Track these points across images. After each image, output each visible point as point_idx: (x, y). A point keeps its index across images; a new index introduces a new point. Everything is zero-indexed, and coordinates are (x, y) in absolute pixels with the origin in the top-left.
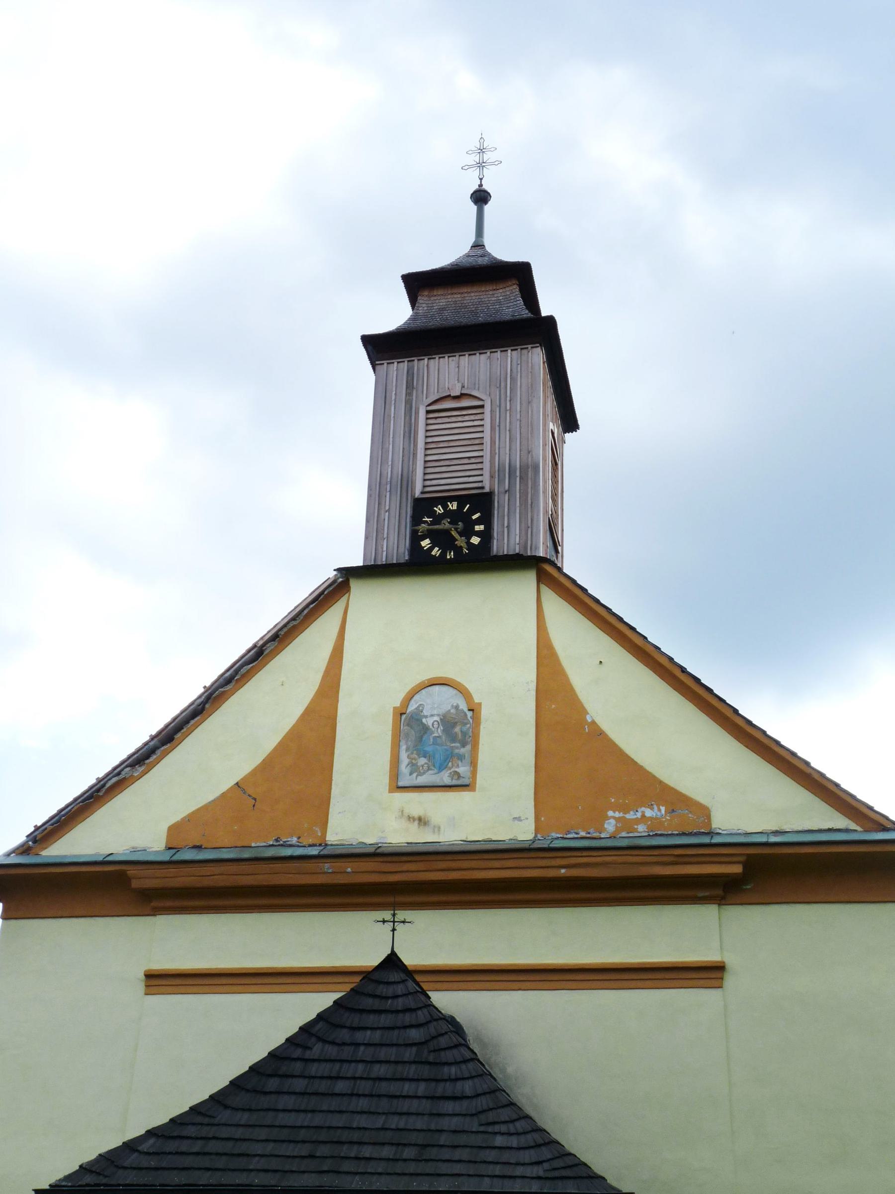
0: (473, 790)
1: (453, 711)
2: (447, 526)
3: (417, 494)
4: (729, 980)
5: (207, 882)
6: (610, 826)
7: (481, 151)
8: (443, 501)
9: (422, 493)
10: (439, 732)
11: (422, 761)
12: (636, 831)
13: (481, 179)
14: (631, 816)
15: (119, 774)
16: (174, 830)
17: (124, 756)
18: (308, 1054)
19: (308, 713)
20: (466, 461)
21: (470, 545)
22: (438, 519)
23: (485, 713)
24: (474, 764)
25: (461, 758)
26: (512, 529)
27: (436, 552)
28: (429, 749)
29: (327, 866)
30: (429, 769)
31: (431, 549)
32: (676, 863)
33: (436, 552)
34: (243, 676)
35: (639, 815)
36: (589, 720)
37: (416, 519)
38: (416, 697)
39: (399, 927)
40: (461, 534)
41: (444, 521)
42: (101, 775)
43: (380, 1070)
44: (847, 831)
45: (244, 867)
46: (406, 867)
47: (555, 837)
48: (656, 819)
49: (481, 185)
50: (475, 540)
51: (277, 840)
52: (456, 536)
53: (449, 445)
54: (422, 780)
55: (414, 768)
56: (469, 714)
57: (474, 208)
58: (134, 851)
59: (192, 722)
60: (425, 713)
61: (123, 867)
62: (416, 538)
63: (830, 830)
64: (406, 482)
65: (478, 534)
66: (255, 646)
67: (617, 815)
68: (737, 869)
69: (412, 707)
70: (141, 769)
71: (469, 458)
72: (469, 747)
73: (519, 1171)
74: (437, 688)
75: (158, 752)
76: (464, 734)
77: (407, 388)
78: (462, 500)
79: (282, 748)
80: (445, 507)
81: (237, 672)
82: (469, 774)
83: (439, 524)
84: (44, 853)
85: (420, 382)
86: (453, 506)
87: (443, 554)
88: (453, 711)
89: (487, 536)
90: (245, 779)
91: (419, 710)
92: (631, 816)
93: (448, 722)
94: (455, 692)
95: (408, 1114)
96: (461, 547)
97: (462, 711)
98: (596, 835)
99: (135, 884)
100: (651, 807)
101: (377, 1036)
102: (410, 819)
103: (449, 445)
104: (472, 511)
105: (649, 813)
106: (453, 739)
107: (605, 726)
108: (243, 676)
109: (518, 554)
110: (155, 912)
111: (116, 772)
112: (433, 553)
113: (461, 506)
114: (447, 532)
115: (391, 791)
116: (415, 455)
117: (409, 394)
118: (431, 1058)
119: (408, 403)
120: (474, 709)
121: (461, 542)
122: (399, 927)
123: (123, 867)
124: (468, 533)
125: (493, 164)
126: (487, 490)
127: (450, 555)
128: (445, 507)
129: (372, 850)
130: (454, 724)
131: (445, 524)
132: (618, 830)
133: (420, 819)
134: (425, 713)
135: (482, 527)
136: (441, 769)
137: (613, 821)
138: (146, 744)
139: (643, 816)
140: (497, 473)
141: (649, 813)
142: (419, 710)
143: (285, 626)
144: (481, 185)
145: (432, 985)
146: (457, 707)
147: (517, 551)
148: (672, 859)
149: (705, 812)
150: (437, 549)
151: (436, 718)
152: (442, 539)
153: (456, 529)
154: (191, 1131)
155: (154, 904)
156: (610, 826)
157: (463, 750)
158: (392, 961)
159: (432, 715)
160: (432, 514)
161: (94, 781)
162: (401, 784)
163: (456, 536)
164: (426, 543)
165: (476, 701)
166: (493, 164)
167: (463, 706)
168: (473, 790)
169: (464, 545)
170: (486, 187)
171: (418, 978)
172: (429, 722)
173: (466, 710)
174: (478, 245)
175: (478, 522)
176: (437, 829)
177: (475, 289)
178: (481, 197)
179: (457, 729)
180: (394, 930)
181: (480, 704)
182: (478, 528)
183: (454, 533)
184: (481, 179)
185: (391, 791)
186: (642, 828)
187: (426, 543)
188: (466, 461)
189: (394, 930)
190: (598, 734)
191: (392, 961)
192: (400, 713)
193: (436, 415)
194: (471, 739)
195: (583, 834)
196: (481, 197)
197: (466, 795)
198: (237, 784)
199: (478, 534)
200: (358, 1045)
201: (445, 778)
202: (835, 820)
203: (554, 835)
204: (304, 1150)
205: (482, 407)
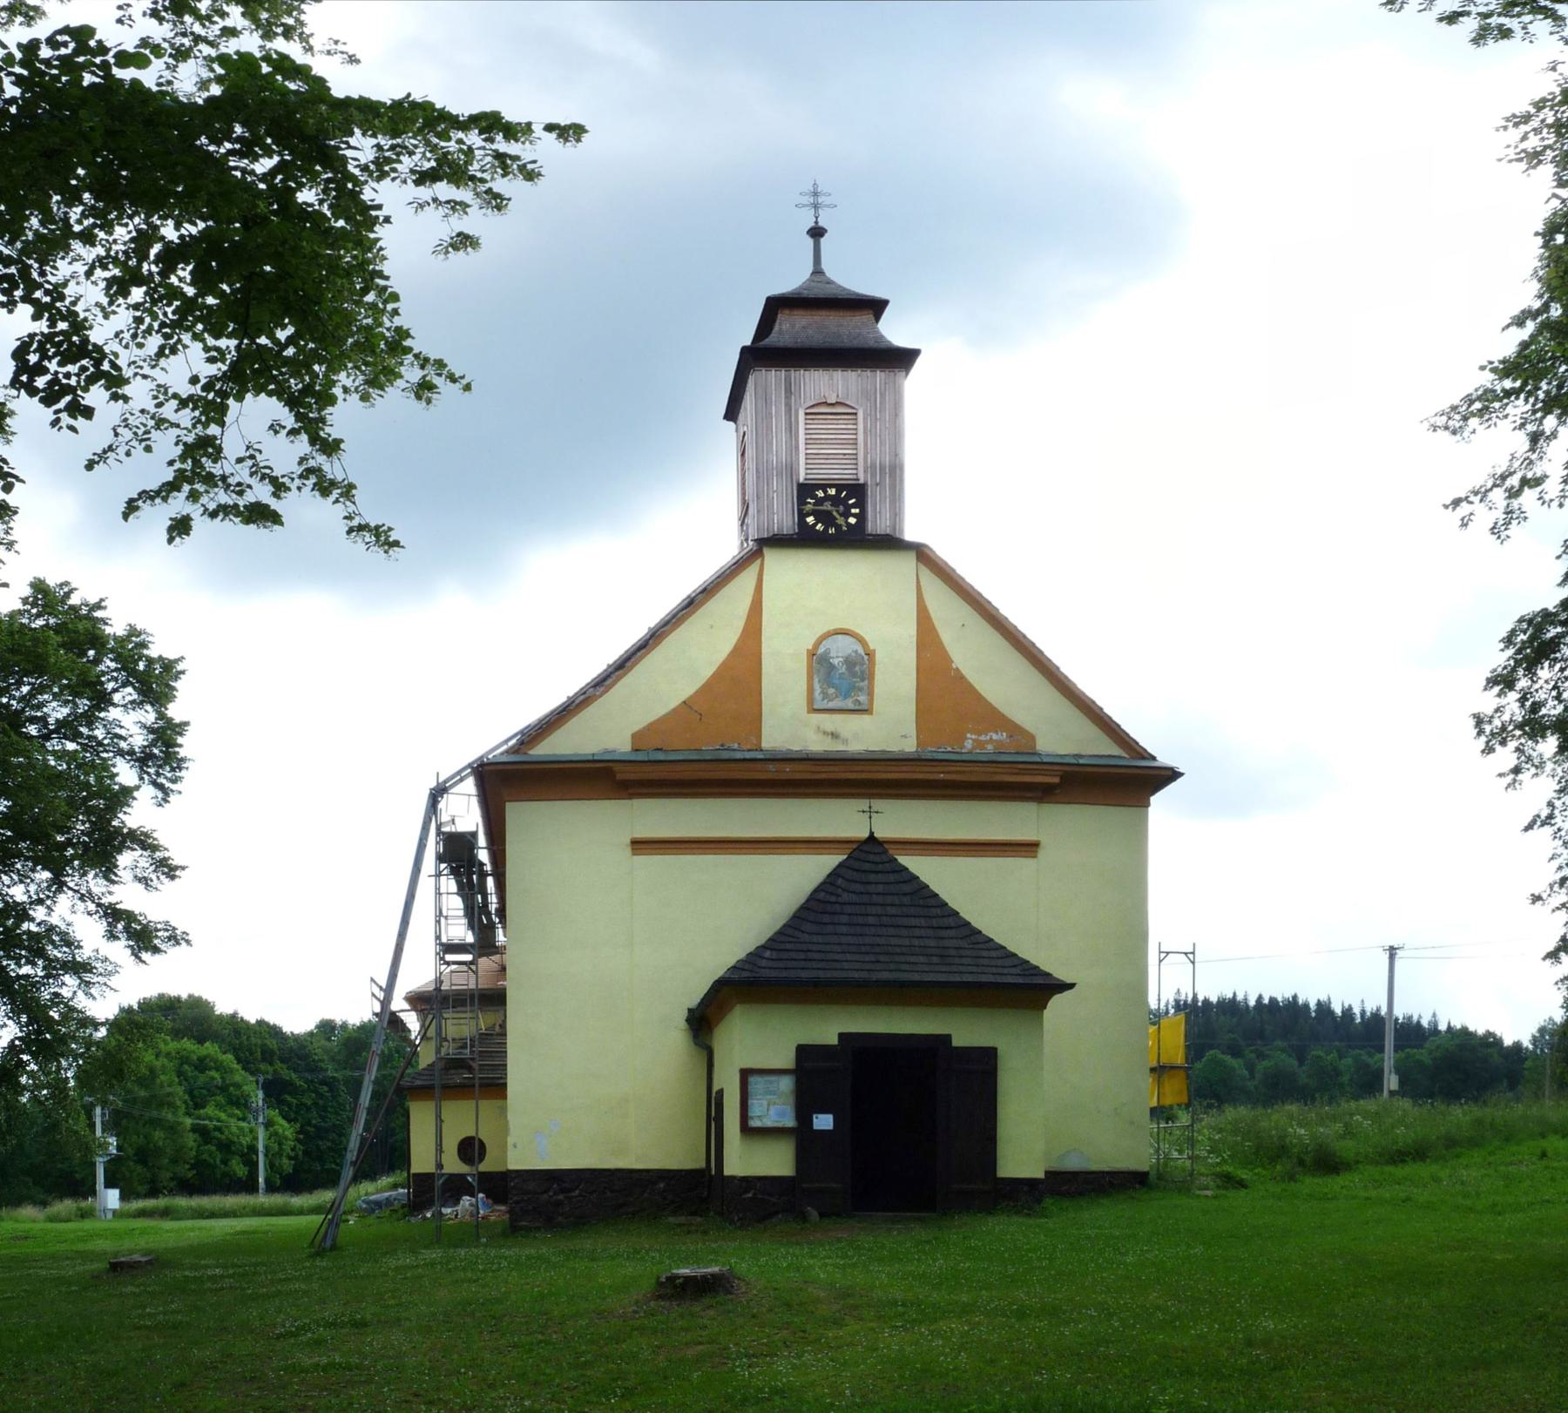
0: (871, 713)
1: (853, 654)
2: (830, 508)
3: (801, 480)
4: (1041, 853)
5: (677, 776)
6: (969, 744)
7: (815, 194)
8: (824, 487)
9: (806, 479)
10: (843, 670)
11: (831, 691)
12: (986, 749)
13: (817, 218)
14: (983, 738)
15: (585, 693)
16: (635, 736)
17: (589, 680)
18: (840, 900)
19: (736, 651)
20: (841, 457)
21: (849, 525)
22: (819, 501)
23: (878, 657)
24: (871, 694)
25: (860, 689)
26: (883, 515)
27: (819, 527)
28: (836, 682)
29: (771, 767)
30: (837, 697)
31: (815, 525)
32: (1017, 774)
33: (819, 527)
34: (678, 619)
35: (988, 737)
36: (954, 666)
37: (801, 501)
38: (824, 643)
39: (873, 815)
40: (841, 515)
41: (826, 503)
42: (571, 694)
43: (893, 911)
44: (1119, 757)
45: (703, 766)
46: (831, 769)
47: (930, 751)
48: (1000, 741)
49: (816, 222)
50: (852, 520)
51: (722, 745)
52: (838, 516)
53: (827, 442)
54: (831, 705)
55: (825, 696)
56: (866, 657)
57: (810, 242)
58: (607, 752)
59: (639, 654)
60: (832, 655)
61: (610, 764)
62: (802, 515)
63: (1109, 756)
64: (791, 469)
65: (854, 515)
66: (689, 597)
67: (973, 737)
68: (1056, 780)
69: (821, 650)
70: (602, 689)
71: (845, 454)
72: (866, 682)
73: (1006, 971)
74: (840, 636)
75: (614, 677)
76: (862, 672)
77: (786, 393)
78: (840, 488)
79: (718, 676)
80: (825, 492)
81: (674, 616)
82: (866, 702)
83: (822, 505)
84: (531, 752)
85: (798, 388)
86: (832, 492)
87: (826, 530)
88: (853, 654)
89: (862, 518)
90: (691, 697)
91: (827, 652)
92: (983, 738)
93: (850, 662)
94: (854, 640)
95: (921, 937)
96: (841, 525)
97: (860, 655)
98: (958, 750)
99: (619, 777)
100: (996, 733)
101: (880, 888)
102: (825, 733)
103: (827, 442)
104: (848, 497)
105: (995, 737)
106: (854, 675)
107: (965, 672)
108: (678, 619)
109: (887, 535)
110: (631, 796)
111: (583, 692)
112: (817, 528)
113: (839, 492)
114: (829, 513)
115: (808, 712)
116: (797, 447)
117: (788, 397)
118: (921, 902)
119: (788, 406)
120: (870, 654)
121: (841, 521)
122: (873, 815)
123: (610, 764)
124: (847, 514)
125: (828, 206)
126: (862, 481)
127: (832, 531)
128: (825, 492)
129: (805, 756)
130: (855, 664)
131: (827, 506)
132: (974, 748)
133: (832, 734)
134: (832, 655)
135: (857, 511)
136: (846, 697)
137: (970, 741)
138: (605, 671)
139: (991, 739)
140: (871, 468)
141: (995, 737)
142: (827, 652)
143: (712, 582)
144: (816, 222)
145: (898, 852)
146: (856, 652)
147: (888, 532)
148: (1017, 771)
149: (1032, 738)
150: (820, 525)
151: (841, 659)
152: (821, 516)
153: (837, 511)
154: (427, 1023)
155: (630, 791)
156: (969, 744)
157: (862, 684)
158: (872, 838)
159: (837, 657)
160: (815, 497)
161: (565, 699)
162: (815, 707)
163: (838, 516)
164: (810, 520)
165: (872, 648)
166: (828, 206)
167: (861, 651)
168: (871, 713)
169: (843, 523)
170: (820, 224)
171: (886, 846)
172: (835, 662)
173: (863, 654)
174: (818, 271)
175: (854, 506)
176: (845, 741)
177: (832, 313)
178: (817, 233)
179: (857, 668)
180: (864, 812)
181: (874, 651)
182: (853, 511)
183: (835, 513)
184: (817, 218)
185: (808, 712)
186: (990, 747)
187: (810, 520)
188: (841, 457)
189: (864, 812)
190: (960, 678)
191: (872, 838)
192: (812, 654)
193: (813, 417)
194: (869, 676)
195: (949, 749)
196: (817, 233)
197: (866, 717)
198: (684, 702)
199: (854, 515)
200: (871, 894)
201: (849, 704)
202: (1113, 749)
203: (930, 749)
204: (872, 958)
205: (856, 414)
